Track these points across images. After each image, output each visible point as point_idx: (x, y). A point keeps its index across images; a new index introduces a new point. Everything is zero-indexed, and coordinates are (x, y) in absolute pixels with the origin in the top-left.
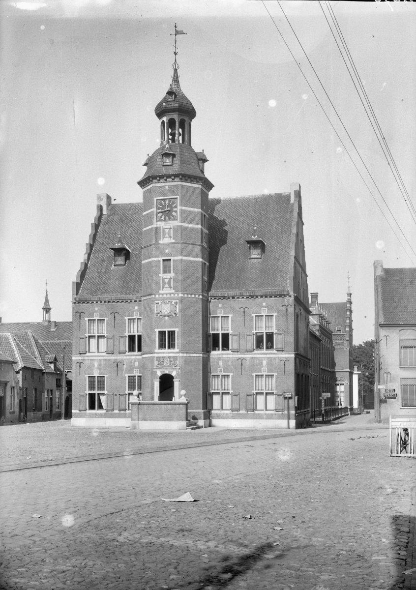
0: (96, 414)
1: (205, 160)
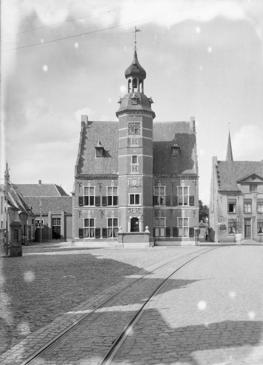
0: (89, 240)
1: (152, 102)
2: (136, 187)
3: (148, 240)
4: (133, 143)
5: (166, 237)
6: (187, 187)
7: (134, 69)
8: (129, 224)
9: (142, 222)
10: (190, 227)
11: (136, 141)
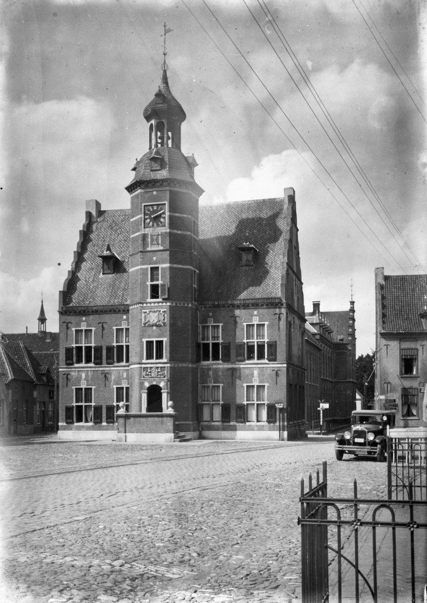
0: (83, 426)
2: (157, 326)
3: (171, 428)
4: (152, 244)
5: (223, 422)
6: (263, 325)
7: (157, 104)
8: (145, 396)
9: (168, 393)
10: (268, 403)
11: (157, 240)
